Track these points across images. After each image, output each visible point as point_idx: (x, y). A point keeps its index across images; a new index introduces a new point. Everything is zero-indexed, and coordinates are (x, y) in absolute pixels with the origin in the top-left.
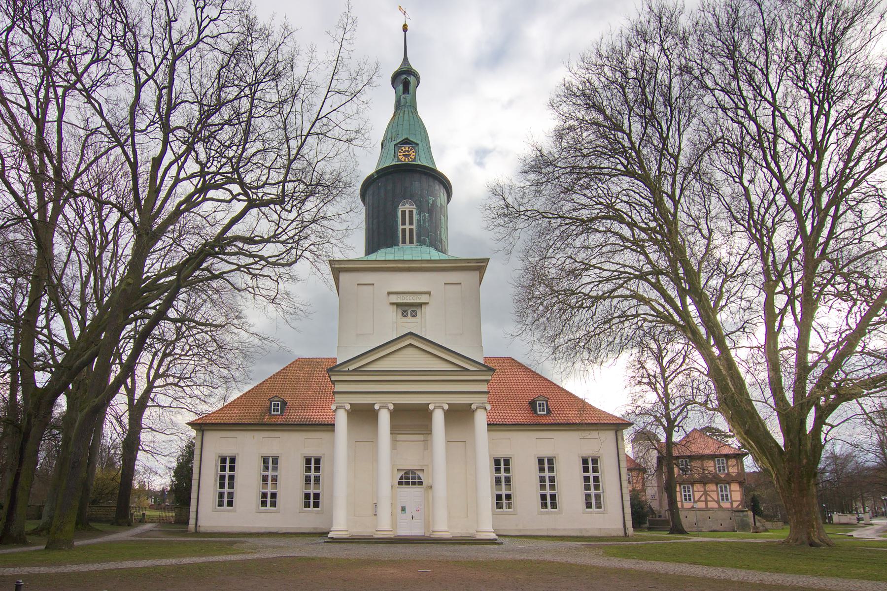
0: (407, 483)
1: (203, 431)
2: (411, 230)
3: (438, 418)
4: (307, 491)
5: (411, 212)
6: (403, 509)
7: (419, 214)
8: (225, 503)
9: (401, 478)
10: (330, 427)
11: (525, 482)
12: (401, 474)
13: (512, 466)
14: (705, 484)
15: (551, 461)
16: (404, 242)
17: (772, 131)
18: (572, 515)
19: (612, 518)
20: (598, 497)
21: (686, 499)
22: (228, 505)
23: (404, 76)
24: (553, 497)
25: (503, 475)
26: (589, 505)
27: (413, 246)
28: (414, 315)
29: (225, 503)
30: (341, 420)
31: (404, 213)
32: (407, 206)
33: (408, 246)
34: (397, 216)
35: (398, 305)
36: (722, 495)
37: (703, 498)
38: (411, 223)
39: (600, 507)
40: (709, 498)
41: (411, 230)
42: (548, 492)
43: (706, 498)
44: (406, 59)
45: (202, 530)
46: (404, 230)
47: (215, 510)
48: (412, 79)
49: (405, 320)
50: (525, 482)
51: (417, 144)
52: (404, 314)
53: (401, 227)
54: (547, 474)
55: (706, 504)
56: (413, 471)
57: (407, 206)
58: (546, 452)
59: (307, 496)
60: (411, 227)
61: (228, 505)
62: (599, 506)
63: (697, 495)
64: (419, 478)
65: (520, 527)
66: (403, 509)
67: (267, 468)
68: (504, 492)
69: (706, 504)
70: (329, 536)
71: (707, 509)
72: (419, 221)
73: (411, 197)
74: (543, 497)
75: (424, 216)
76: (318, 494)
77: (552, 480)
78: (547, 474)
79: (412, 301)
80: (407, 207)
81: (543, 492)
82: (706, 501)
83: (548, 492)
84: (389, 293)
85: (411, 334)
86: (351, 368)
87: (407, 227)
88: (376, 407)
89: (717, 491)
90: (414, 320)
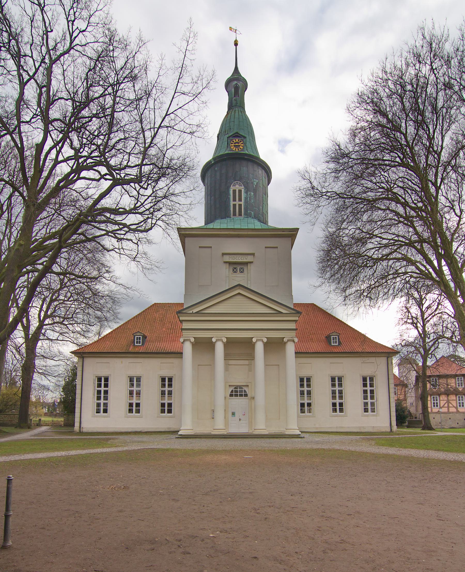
0: (236, 395)
1: (83, 358)
2: (240, 205)
4: (163, 402)
6: (233, 414)
7: (246, 192)
9: (232, 391)
10: (179, 354)
11: (150, 396)
13: (313, 383)
21: (434, 406)
25: (306, 389)
30: (188, 349)
31: (234, 191)
32: (237, 186)
33: (237, 218)
34: (229, 194)
35: (230, 263)
36: (434, 403)
37: (446, 405)
40: (450, 405)
41: (240, 205)
42: (338, 401)
43: (448, 405)
44: (236, 68)
45: (84, 430)
47: (94, 416)
49: (235, 275)
51: (245, 137)
52: (235, 271)
53: (232, 203)
55: (448, 409)
56: (241, 387)
57: (237, 186)
60: (240, 203)
61: (372, 412)
62: (373, 411)
63: (442, 403)
64: (245, 391)
66: (233, 414)
68: (166, 401)
69: (448, 409)
70: (179, 433)
71: (449, 412)
72: (246, 198)
77: (341, 392)
78: (337, 388)
80: (237, 188)
81: (334, 401)
82: (448, 407)
83: (338, 401)
85: (239, 285)
86: (195, 311)
88: (214, 340)
89: (456, 400)
90: (242, 275)
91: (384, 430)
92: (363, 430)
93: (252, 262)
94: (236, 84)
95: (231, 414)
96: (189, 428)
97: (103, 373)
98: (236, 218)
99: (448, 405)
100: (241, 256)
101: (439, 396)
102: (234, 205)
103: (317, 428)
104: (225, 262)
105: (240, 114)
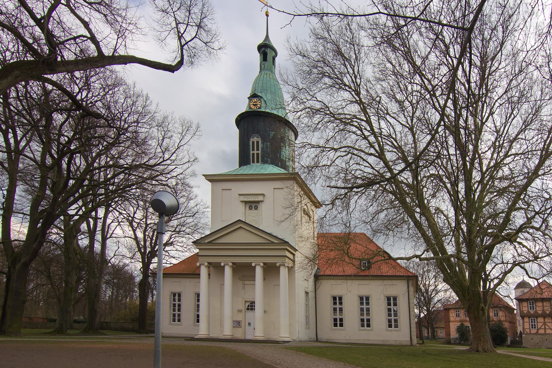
2: (258, 154)
3: (259, 272)
4: (335, 317)
5: (258, 142)
6: (249, 324)
7: (263, 143)
8: (176, 320)
9: (249, 306)
10: (198, 275)
11: (351, 311)
12: (247, 304)
13: (344, 301)
14: (544, 318)
15: (367, 298)
16: (253, 162)
17: (24, 138)
18: (379, 332)
19: (403, 334)
20: (396, 321)
21: (532, 327)
22: (367, 327)
23: (263, 49)
24: (368, 320)
25: (338, 306)
26: (390, 326)
27: (259, 164)
28: (256, 208)
29: (176, 320)
31: (253, 143)
32: (255, 138)
33: (256, 164)
34: (249, 145)
35: (246, 202)
36: (532, 325)
37: (543, 327)
38: (258, 150)
39: (370, 327)
40: (547, 327)
41: (258, 154)
42: (365, 317)
43: (545, 327)
44: (267, 36)
46: (253, 154)
47: (170, 324)
48: (268, 51)
49: (251, 211)
50: (351, 311)
51: (261, 97)
52: (251, 208)
53: (251, 152)
54: (365, 306)
55: (545, 331)
57: (255, 138)
58: (364, 292)
59: (335, 320)
60: (258, 152)
61: (367, 327)
62: (396, 326)
63: (540, 325)
65: (347, 338)
66: (249, 324)
67: (174, 300)
68: (338, 317)
69: (545, 331)
71: (545, 334)
72: (262, 148)
73: (258, 133)
74: (362, 320)
75: (267, 145)
76: (369, 319)
77: (368, 310)
78: (365, 306)
79: (253, 200)
80: (255, 139)
81: (362, 317)
82: (545, 329)
83: (365, 317)
84: (240, 195)
85: (239, 220)
86: (206, 241)
87: (255, 152)
88: (253, 265)
89: (529, 322)
90: (256, 211)
91: (405, 344)
92: (387, 343)
93: (262, 201)
94: (264, 50)
95: (247, 324)
96: (204, 333)
97: (177, 290)
98: (254, 165)
99: (545, 327)
100: (253, 196)
101: (537, 319)
102: (253, 154)
103: (347, 340)
104: (242, 201)
105: (265, 76)
